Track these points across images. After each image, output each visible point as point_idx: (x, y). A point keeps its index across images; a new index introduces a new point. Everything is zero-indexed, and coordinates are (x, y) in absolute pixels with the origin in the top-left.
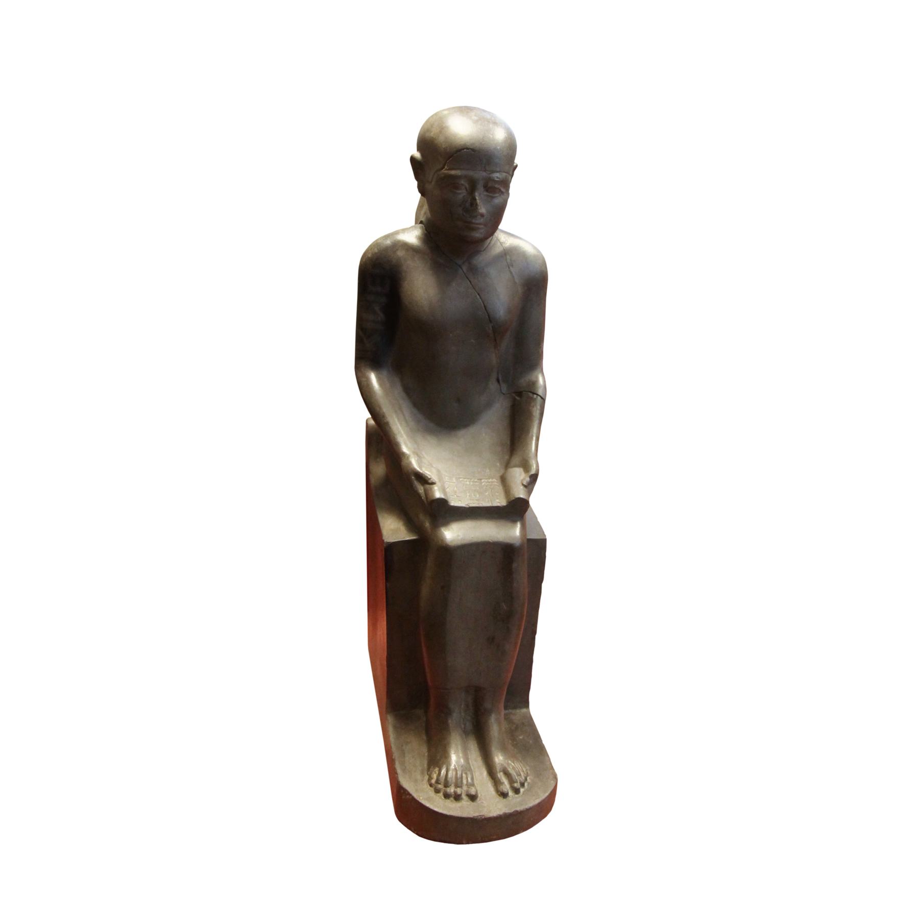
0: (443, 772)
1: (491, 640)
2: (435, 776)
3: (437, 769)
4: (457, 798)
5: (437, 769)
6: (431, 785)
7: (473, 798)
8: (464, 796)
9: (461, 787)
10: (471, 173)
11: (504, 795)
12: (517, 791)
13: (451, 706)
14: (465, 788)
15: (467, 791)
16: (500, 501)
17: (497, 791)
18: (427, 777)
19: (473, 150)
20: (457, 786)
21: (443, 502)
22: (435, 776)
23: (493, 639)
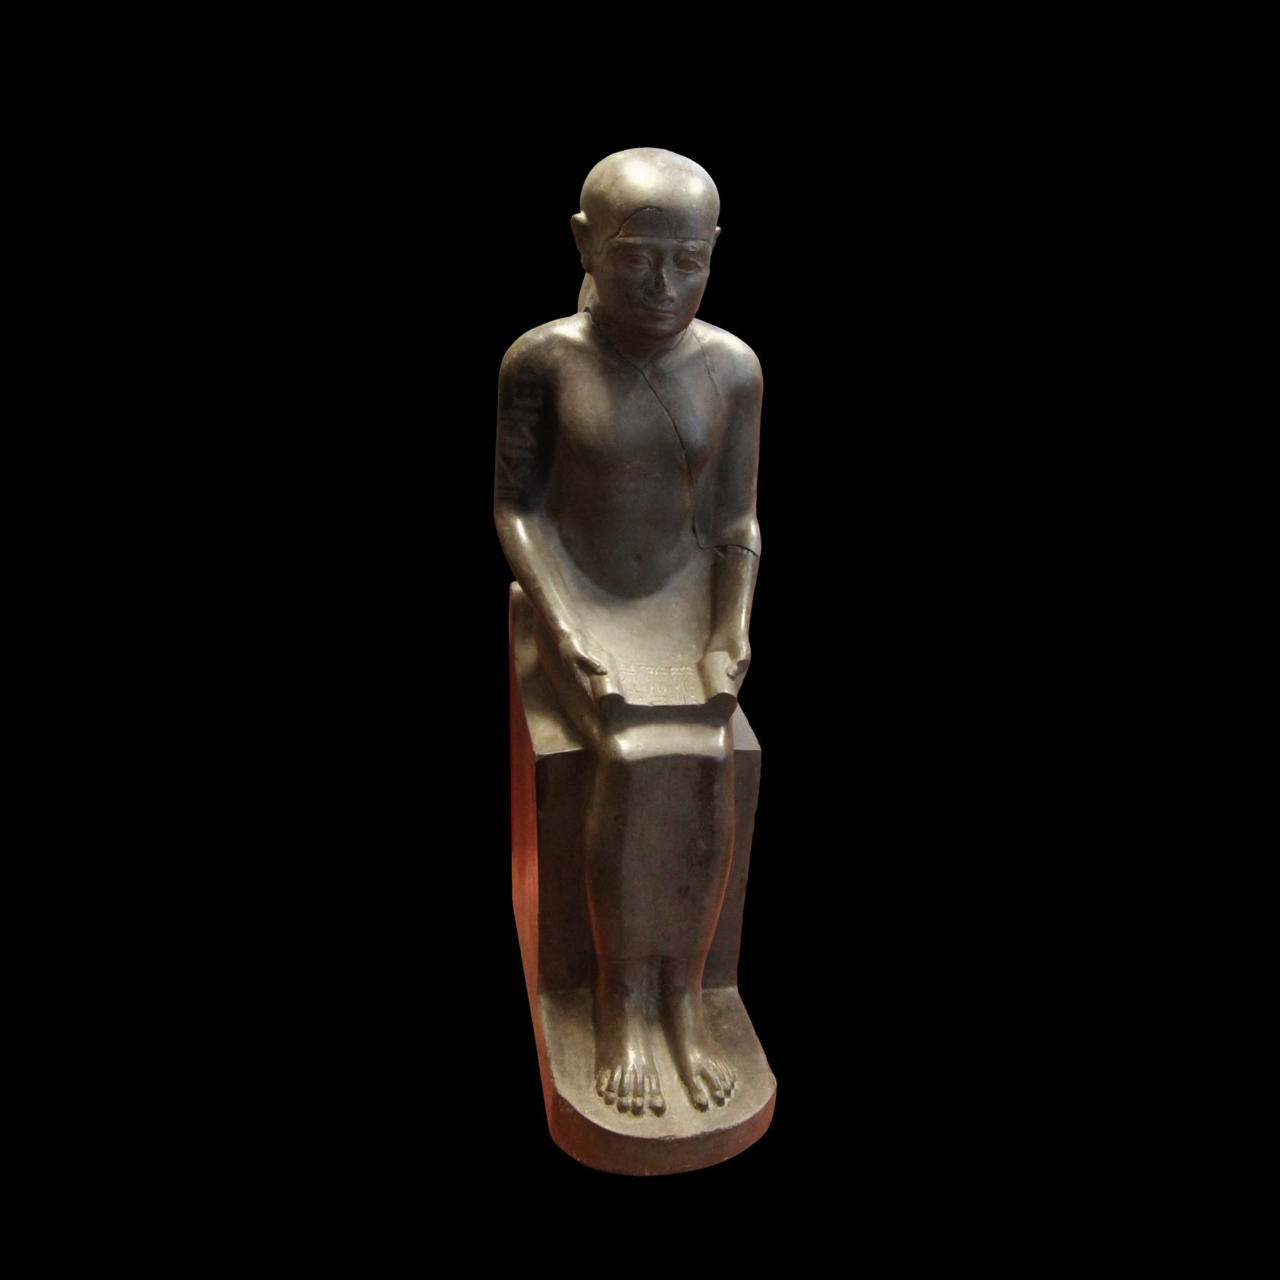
0: (617, 1075)
1: (684, 891)
2: (606, 1081)
3: (608, 1071)
4: (637, 1111)
5: (608, 1071)
6: (600, 1094)
7: (658, 1111)
8: (646, 1109)
9: (642, 1096)
10: (656, 241)
11: (702, 1107)
12: (720, 1102)
13: (628, 983)
14: (647, 1097)
15: (651, 1102)
16: (696, 698)
17: (692, 1101)
18: (594, 1083)
19: (659, 209)
20: (636, 1095)
21: (617, 700)
22: (606, 1081)
23: (687, 889)
